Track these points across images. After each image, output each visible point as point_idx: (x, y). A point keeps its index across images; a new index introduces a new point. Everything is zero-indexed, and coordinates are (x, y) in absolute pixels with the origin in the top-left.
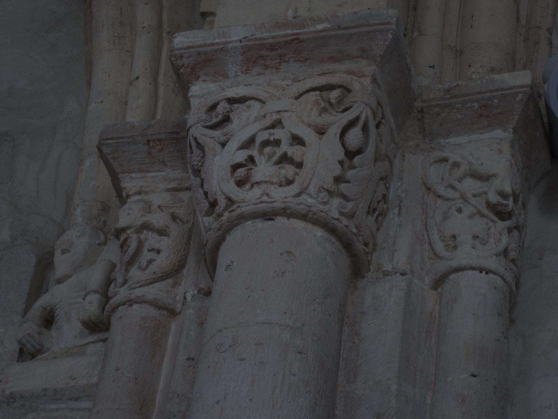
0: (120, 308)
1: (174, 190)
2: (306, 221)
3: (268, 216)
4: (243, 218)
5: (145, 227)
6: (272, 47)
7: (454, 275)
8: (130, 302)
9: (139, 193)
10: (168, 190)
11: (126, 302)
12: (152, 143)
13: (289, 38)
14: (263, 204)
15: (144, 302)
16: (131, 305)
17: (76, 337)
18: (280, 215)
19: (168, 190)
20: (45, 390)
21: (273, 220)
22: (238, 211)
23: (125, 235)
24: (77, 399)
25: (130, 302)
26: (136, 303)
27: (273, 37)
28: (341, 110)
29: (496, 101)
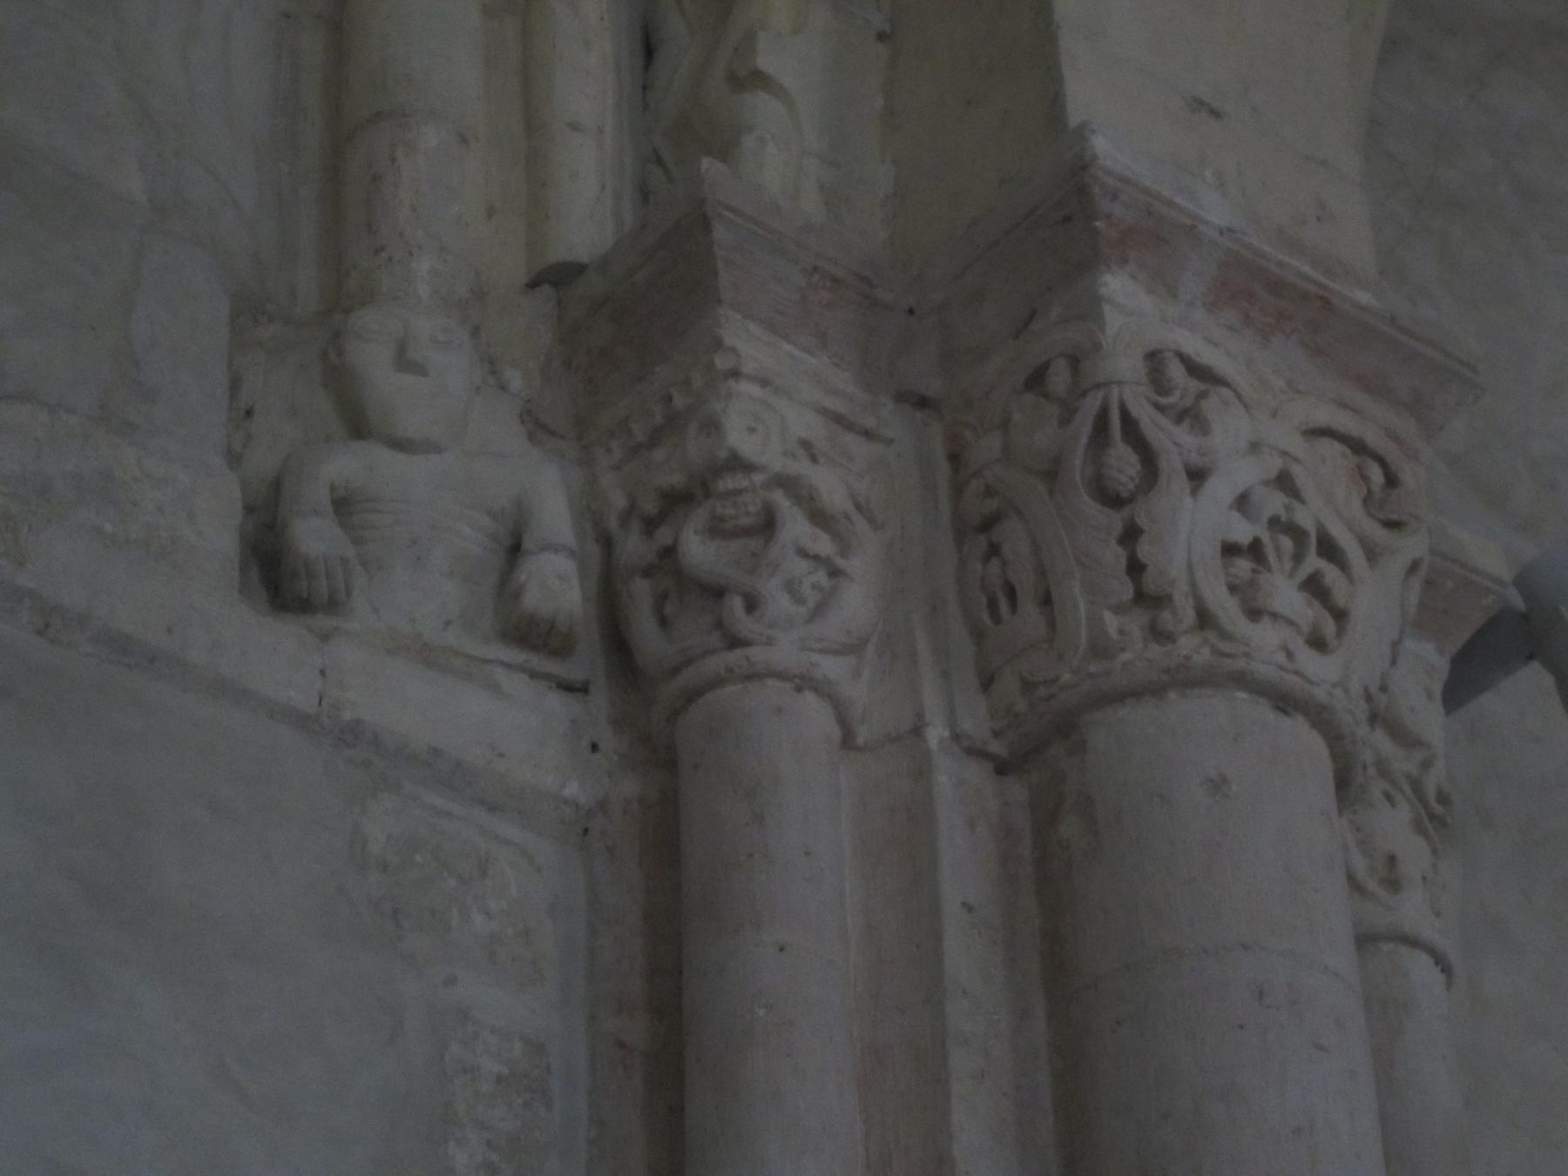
0: (770, 682)
1: (838, 419)
2: (1331, 747)
3: (1284, 702)
4: (1242, 680)
5: (786, 483)
6: (1277, 286)
7: (1392, 946)
8: (804, 682)
9: (765, 383)
10: (824, 412)
11: (795, 676)
12: (817, 277)
13: (1313, 289)
14: (1296, 679)
15: (829, 696)
16: (799, 689)
17: (448, 623)
18: (1307, 715)
19: (824, 412)
20: (437, 752)
21: (1285, 712)
22: (1240, 664)
23: (745, 483)
24: (493, 809)
25: (804, 682)
26: (816, 690)
27: (1280, 264)
28: (1381, 516)
29: (1450, 584)
